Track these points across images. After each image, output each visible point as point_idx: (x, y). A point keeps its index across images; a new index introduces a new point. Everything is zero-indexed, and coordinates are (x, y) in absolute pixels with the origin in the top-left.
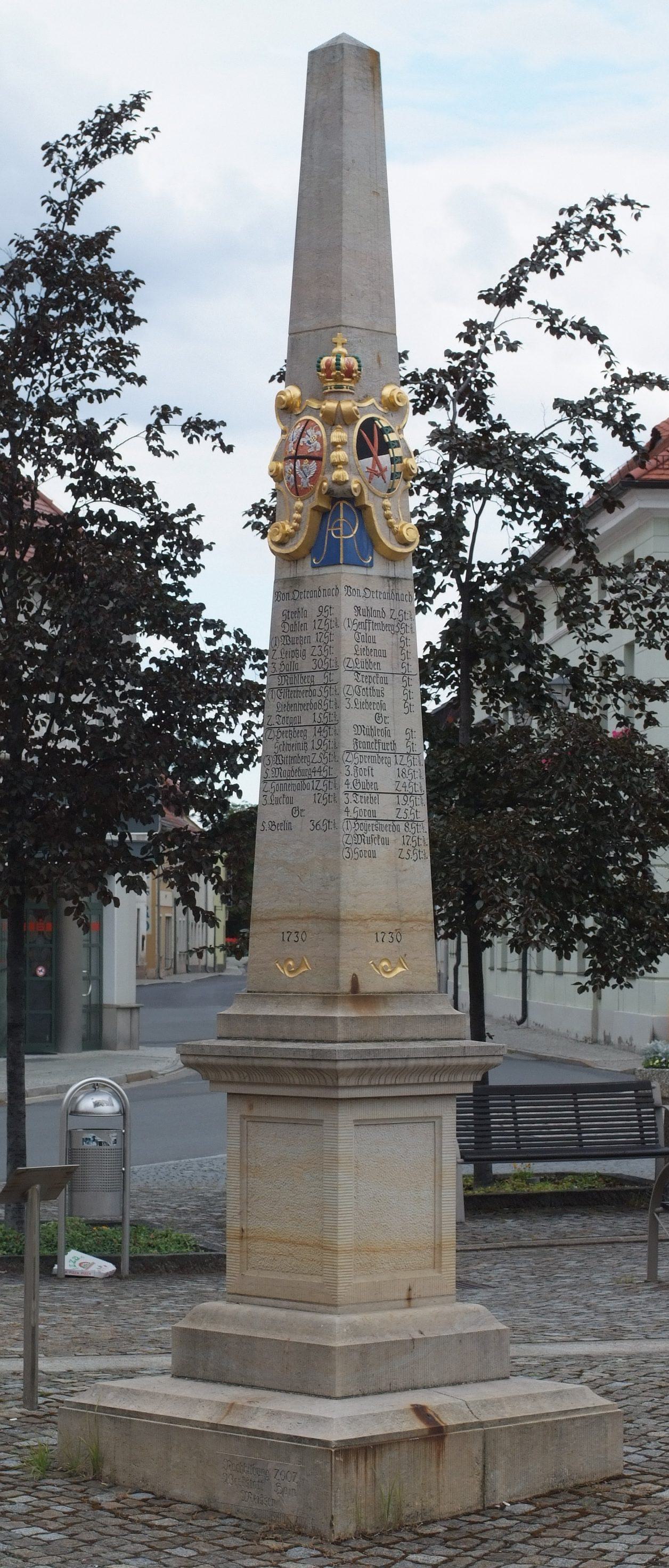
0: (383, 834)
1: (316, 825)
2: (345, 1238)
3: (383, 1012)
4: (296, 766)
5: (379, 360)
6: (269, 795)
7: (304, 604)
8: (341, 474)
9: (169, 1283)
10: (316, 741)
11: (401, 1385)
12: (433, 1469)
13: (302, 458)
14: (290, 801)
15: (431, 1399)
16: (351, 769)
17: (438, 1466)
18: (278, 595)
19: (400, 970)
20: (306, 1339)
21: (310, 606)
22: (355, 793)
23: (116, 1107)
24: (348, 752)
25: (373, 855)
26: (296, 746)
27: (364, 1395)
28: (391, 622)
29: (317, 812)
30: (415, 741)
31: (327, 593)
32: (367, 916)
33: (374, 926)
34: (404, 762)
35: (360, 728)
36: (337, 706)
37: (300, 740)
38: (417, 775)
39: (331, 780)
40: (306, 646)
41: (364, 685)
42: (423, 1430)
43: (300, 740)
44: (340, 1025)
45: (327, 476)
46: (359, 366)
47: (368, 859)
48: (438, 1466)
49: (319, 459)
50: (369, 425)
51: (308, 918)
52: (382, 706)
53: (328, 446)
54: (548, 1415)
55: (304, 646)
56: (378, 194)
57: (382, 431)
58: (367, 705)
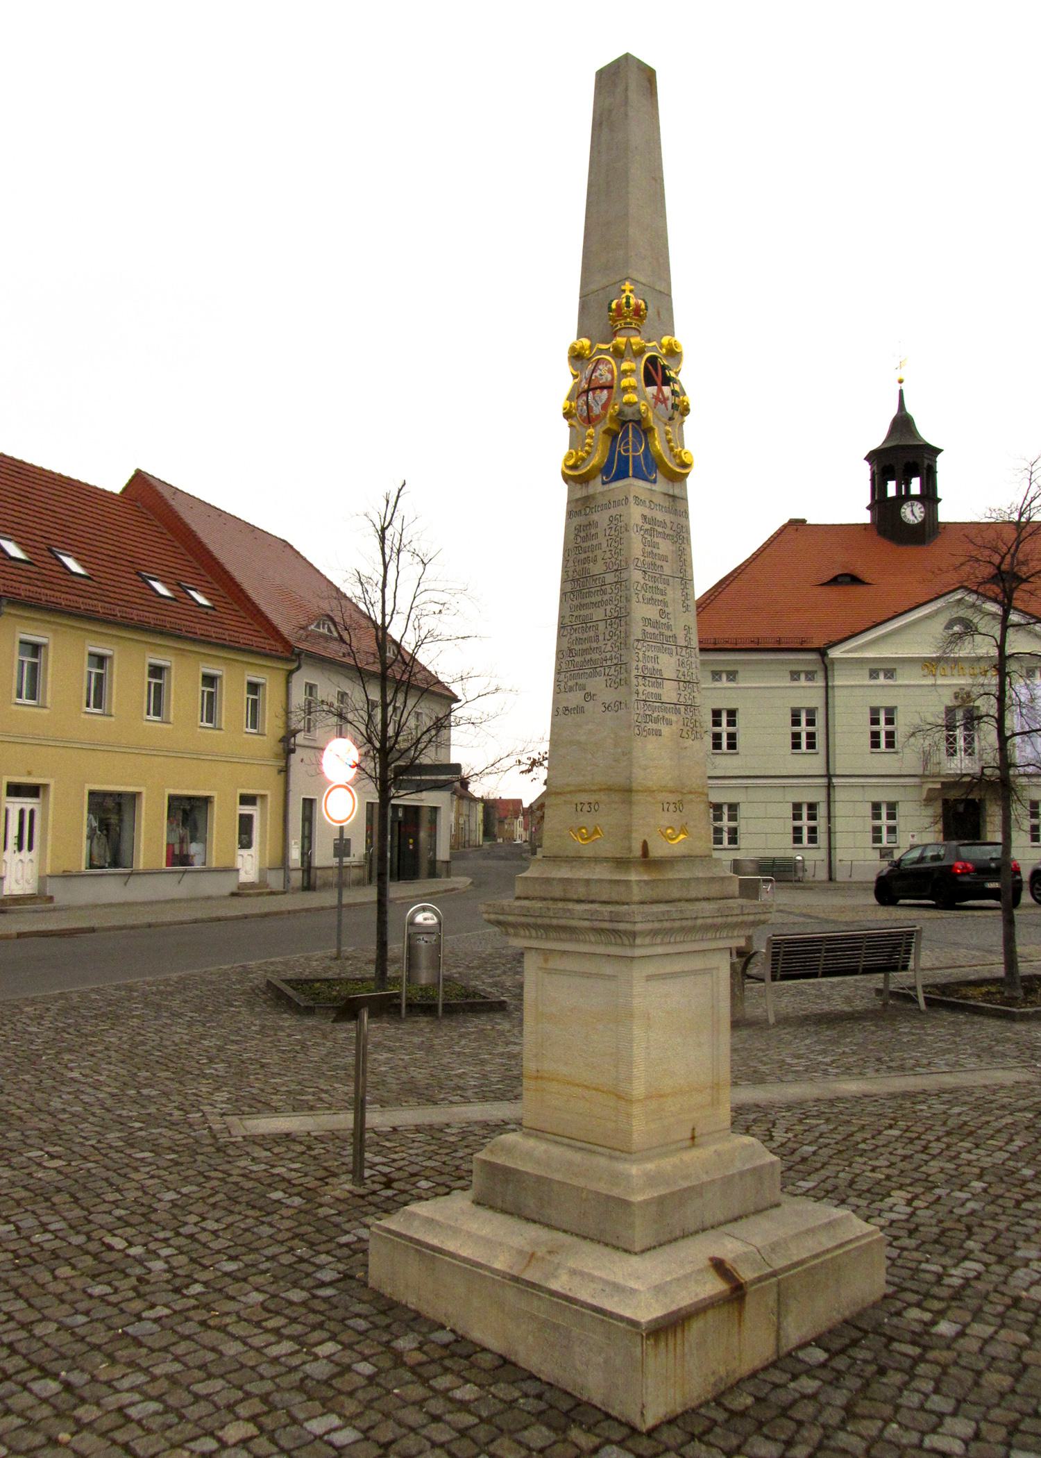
0: (667, 716)
1: (607, 708)
2: (638, 1089)
3: (670, 875)
4: (588, 657)
5: (659, 314)
6: (563, 684)
7: (595, 517)
8: (631, 397)
9: (465, 1021)
10: (607, 633)
11: (693, 1228)
12: (736, 1330)
13: (594, 389)
14: (583, 688)
15: (728, 1247)
16: (641, 656)
17: (740, 1326)
18: (570, 514)
19: (682, 836)
20: (603, 1188)
21: (602, 518)
22: (644, 677)
23: (435, 920)
24: (638, 640)
25: (658, 733)
26: (589, 640)
27: (661, 1245)
28: (671, 532)
29: (609, 696)
30: (692, 636)
31: (617, 503)
32: (655, 788)
33: (660, 797)
34: (684, 653)
35: (647, 621)
36: (628, 600)
37: (592, 634)
38: (694, 666)
39: (622, 665)
40: (598, 552)
41: (651, 584)
42: (725, 1291)
43: (592, 634)
44: (635, 889)
45: (618, 401)
46: (646, 306)
47: (655, 737)
48: (740, 1326)
49: (610, 387)
50: (653, 361)
51: (600, 790)
52: (666, 604)
53: (619, 375)
54: (828, 1251)
55: (595, 553)
56: (656, 180)
57: (664, 368)
58: (651, 601)
